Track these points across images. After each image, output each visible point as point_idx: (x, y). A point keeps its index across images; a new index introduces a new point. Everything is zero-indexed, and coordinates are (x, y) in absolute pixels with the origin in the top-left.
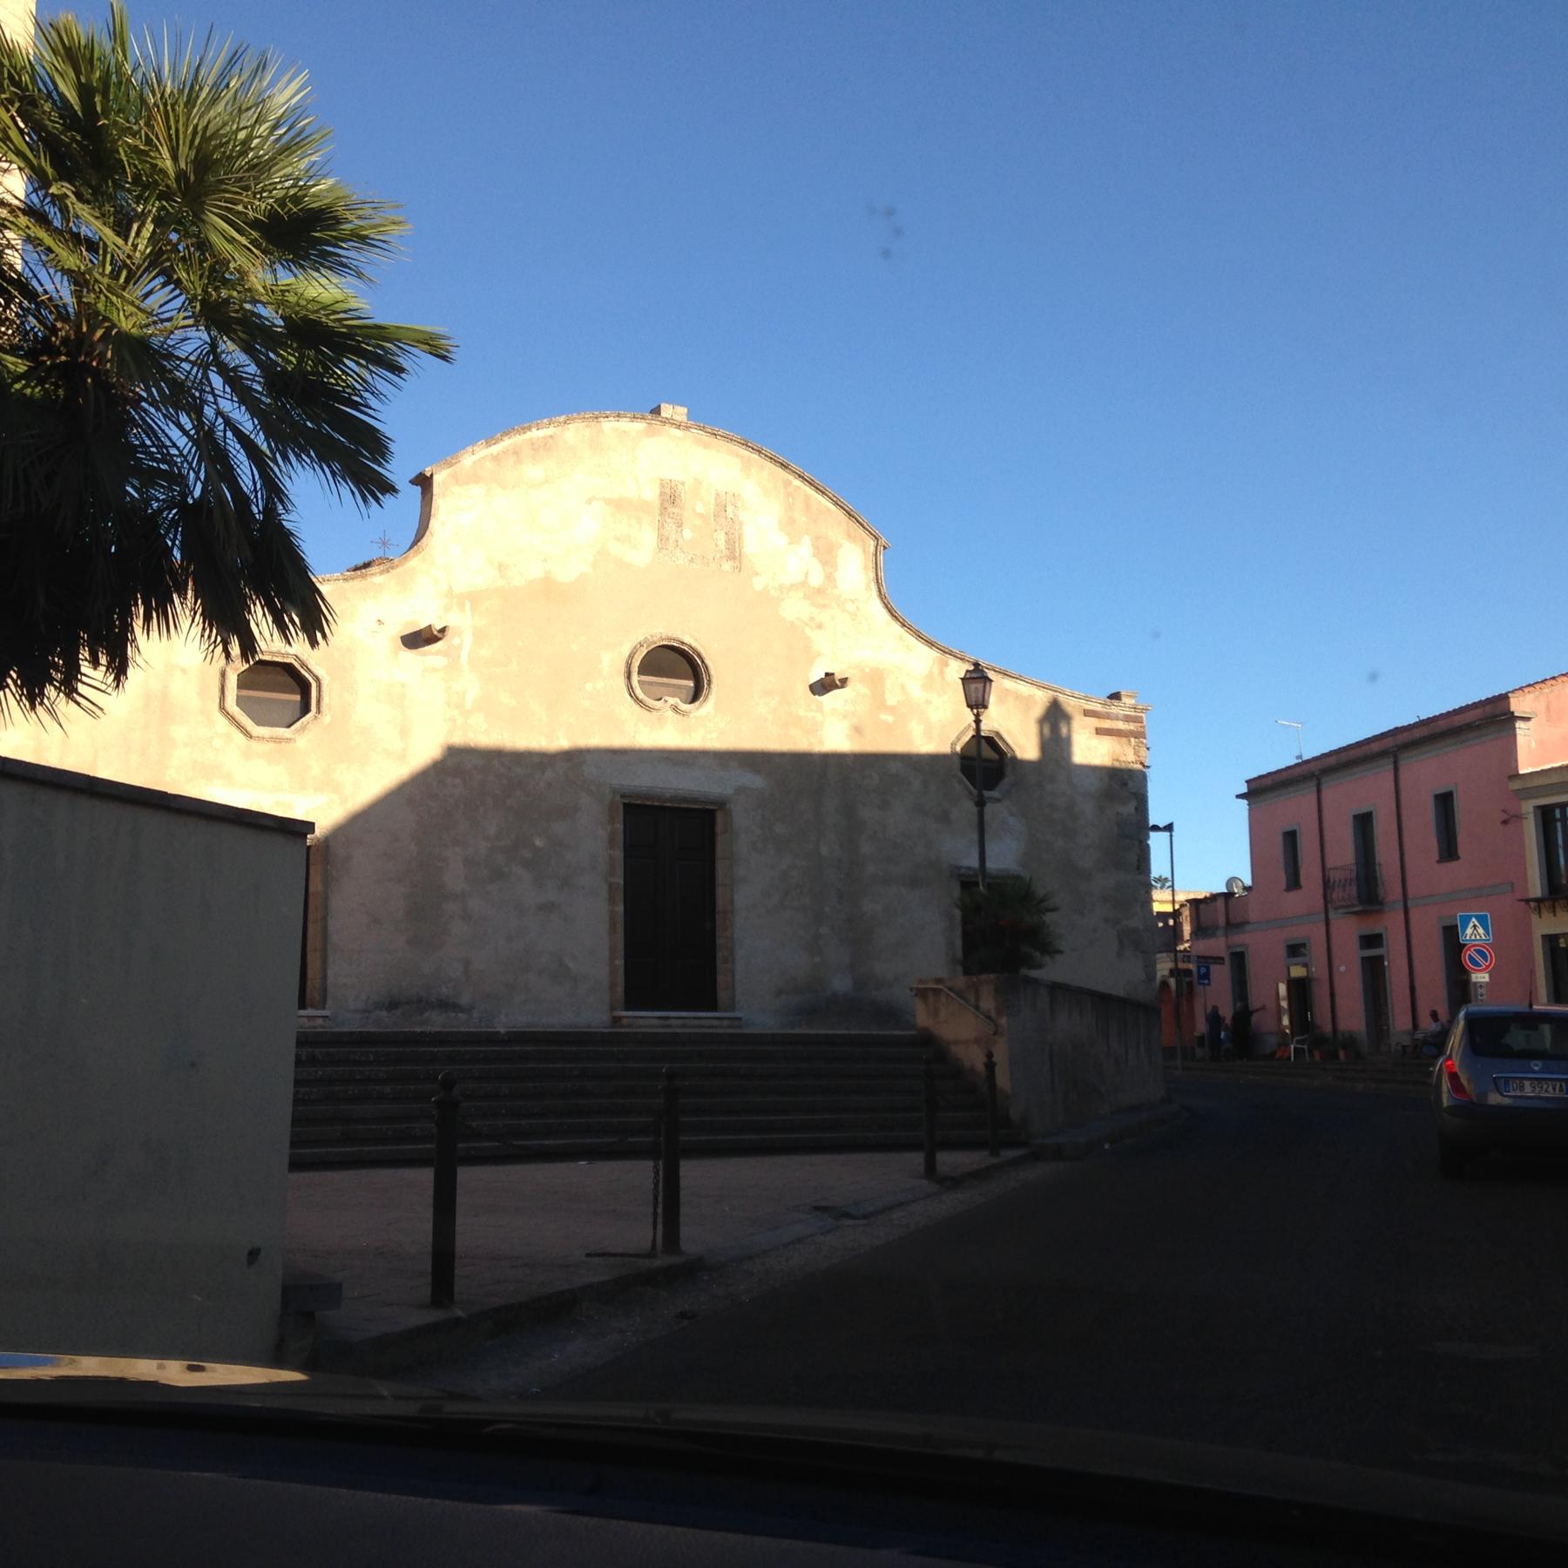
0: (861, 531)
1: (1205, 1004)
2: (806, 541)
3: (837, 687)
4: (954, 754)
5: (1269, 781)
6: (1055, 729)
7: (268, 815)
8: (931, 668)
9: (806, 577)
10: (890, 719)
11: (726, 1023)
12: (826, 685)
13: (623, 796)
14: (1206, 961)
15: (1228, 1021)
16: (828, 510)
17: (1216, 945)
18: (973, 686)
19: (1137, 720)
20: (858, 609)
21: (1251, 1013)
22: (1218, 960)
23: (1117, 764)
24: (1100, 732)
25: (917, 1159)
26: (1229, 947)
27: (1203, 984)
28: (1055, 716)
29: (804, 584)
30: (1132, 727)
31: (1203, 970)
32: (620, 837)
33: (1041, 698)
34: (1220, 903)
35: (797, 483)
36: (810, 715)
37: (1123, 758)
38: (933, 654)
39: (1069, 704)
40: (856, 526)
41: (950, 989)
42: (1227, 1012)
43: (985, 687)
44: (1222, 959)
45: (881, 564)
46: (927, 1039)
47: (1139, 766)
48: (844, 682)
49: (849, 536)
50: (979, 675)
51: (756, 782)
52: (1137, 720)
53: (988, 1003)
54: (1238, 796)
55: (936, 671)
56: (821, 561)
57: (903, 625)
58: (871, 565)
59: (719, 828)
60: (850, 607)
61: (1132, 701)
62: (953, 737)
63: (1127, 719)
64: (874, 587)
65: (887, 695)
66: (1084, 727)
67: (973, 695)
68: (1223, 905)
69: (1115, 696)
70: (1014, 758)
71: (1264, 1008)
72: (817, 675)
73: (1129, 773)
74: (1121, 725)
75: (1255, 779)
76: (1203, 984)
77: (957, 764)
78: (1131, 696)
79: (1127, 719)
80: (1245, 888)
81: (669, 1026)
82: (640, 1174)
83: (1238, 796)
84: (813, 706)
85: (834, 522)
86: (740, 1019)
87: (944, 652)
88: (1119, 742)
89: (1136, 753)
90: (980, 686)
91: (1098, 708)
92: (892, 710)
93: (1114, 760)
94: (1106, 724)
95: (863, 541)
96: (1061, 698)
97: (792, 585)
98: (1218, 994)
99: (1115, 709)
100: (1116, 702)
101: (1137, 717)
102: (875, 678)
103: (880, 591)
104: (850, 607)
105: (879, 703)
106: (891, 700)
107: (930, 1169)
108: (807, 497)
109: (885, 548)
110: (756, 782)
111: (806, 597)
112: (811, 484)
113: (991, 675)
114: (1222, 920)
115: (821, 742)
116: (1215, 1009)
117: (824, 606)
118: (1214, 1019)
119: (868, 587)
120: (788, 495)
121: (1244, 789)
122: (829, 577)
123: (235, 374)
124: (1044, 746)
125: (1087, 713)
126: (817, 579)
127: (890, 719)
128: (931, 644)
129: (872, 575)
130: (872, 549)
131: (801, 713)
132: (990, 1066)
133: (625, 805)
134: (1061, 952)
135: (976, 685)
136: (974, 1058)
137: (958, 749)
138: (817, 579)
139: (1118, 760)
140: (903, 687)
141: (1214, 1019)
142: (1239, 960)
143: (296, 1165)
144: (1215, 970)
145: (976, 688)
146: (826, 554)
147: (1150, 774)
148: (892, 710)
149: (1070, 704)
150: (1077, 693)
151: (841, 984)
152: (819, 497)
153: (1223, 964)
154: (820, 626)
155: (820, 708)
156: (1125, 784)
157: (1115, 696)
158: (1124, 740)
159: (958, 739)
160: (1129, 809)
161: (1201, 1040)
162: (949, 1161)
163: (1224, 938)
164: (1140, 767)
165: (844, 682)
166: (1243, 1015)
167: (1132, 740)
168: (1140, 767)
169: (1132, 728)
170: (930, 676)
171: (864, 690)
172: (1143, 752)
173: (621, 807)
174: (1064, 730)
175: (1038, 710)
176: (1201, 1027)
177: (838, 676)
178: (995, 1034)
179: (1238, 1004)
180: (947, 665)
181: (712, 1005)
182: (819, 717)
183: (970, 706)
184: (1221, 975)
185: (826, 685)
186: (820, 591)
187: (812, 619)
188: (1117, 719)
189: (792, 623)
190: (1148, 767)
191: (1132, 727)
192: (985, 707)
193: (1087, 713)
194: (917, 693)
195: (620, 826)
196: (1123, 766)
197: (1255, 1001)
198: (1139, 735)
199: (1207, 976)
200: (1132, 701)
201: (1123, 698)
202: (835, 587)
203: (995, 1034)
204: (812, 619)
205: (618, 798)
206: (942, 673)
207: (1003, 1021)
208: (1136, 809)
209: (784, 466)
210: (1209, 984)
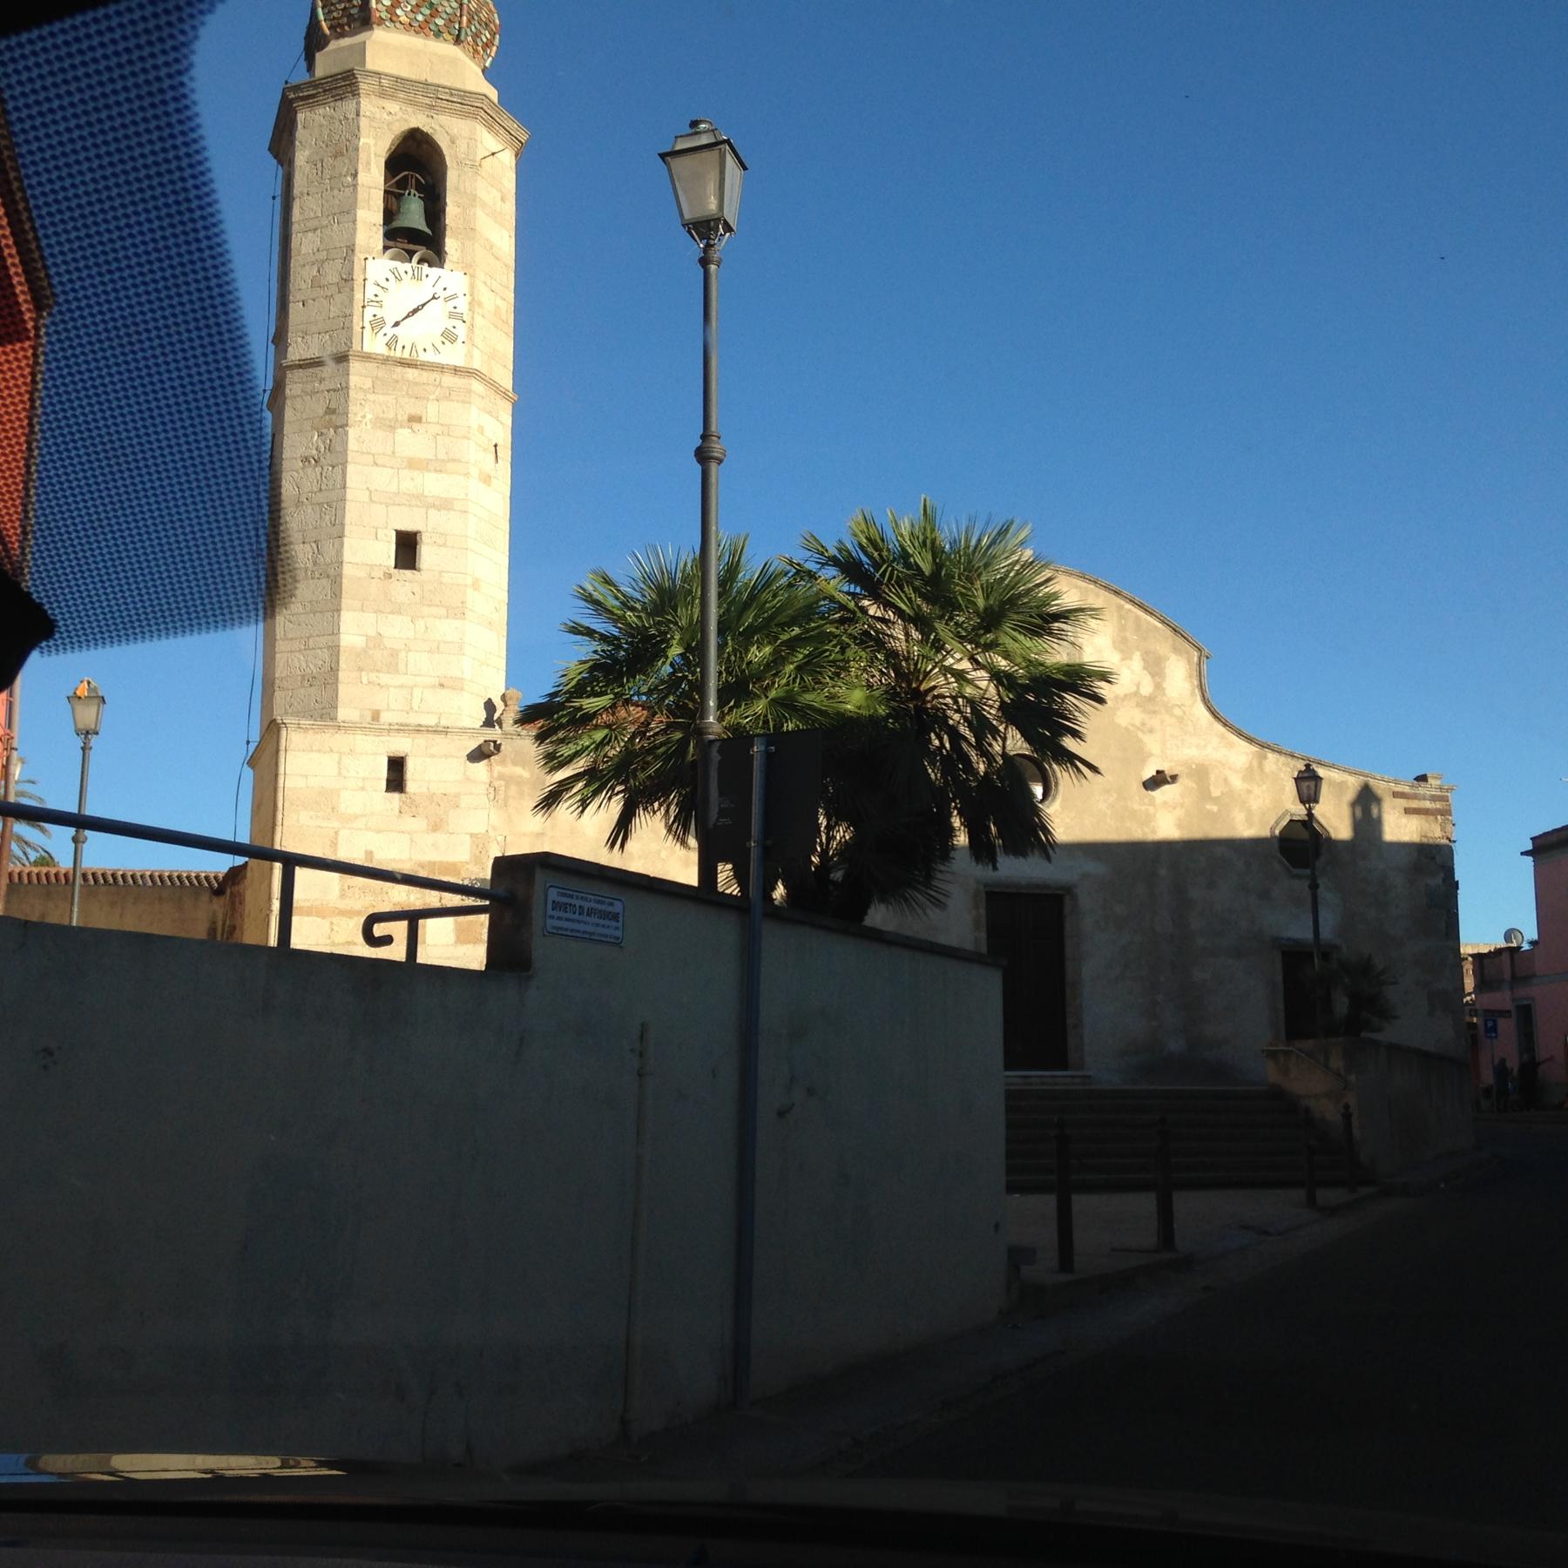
0: (1187, 646)
1: (1493, 1056)
2: (1137, 656)
3: (1168, 783)
4: (1273, 837)
5: (1554, 839)
6: (1367, 812)
7: (150, 839)
8: (1251, 762)
9: (1138, 688)
10: (1215, 808)
11: (1077, 1080)
12: (1158, 781)
13: (986, 885)
14: (1492, 1015)
15: (1515, 1072)
16: (1156, 627)
17: (1501, 999)
18: (1305, 784)
19: (1444, 799)
20: (1184, 713)
21: (1539, 1064)
22: (1504, 1013)
23: (1425, 840)
24: (1408, 811)
25: (1300, 1194)
26: (1513, 1000)
27: (1491, 1037)
28: (1366, 800)
29: (1136, 693)
30: (1438, 805)
31: (1490, 1024)
32: (983, 920)
33: (1353, 783)
34: (1505, 957)
35: (1128, 606)
36: (1143, 808)
37: (1430, 835)
38: (1254, 749)
39: (1379, 787)
40: (1180, 640)
41: (1300, 1050)
42: (1513, 1064)
43: (1316, 786)
44: (1509, 1012)
45: (1205, 672)
46: (1277, 1094)
47: (1445, 841)
48: (1174, 778)
49: (1176, 650)
50: (1311, 774)
51: (1092, 867)
52: (1444, 799)
53: (1337, 1062)
54: (1522, 854)
55: (1255, 764)
56: (1150, 673)
57: (1225, 725)
58: (1195, 674)
59: (1067, 910)
60: (1177, 712)
61: (1438, 782)
62: (1272, 822)
63: (1434, 799)
64: (1197, 692)
65: (1212, 788)
66: (1394, 808)
67: (1305, 791)
68: (1508, 961)
69: (1422, 778)
70: (1329, 839)
71: (1551, 1059)
72: (1149, 773)
73: (1438, 847)
74: (1428, 804)
75: (1540, 836)
76: (1491, 1037)
77: (1276, 845)
78: (1436, 778)
79: (1434, 799)
80: (1532, 943)
81: (1030, 1084)
82: (1146, 1203)
83: (1522, 854)
84: (1146, 801)
85: (1163, 641)
86: (1089, 1076)
87: (1262, 746)
88: (1427, 821)
89: (1443, 829)
90: (1312, 784)
91: (1407, 789)
92: (1216, 800)
93: (1422, 836)
94: (1414, 804)
95: (1188, 653)
96: (1372, 782)
97: (1126, 695)
98: (1505, 1047)
99: (1422, 790)
100: (1422, 784)
101: (1442, 797)
102: (1201, 773)
103: (1203, 696)
104: (1177, 712)
105: (1204, 794)
106: (1216, 792)
107: (1311, 1201)
108: (1137, 618)
109: (1207, 658)
110: (1092, 867)
111: (1138, 705)
112: (1141, 606)
113: (1321, 772)
114: (1507, 975)
115: (1154, 831)
116: (1503, 1061)
117: (1154, 712)
118: (1501, 1071)
119: (1193, 693)
120: (1121, 617)
121: (1530, 847)
122: (1158, 687)
123: (1049, 703)
124: (1357, 826)
125: (1396, 795)
126: (1147, 688)
127: (1215, 808)
128: (1250, 740)
129: (1196, 683)
130: (1196, 659)
131: (1136, 806)
132: (1347, 1116)
133: (987, 893)
134: (1396, 1017)
135: (1308, 784)
136: (1329, 1112)
137: (1277, 832)
138: (1147, 688)
139: (1426, 837)
140: (1226, 780)
141: (1501, 1071)
142: (1525, 1013)
143: (1011, 1188)
144: (1503, 1024)
145: (1308, 787)
146: (1155, 667)
147: (1457, 848)
148: (1216, 800)
149: (1380, 787)
150: (1386, 778)
151: (1175, 1045)
152: (1149, 618)
153: (1511, 1016)
154: (1151, 731)
155: (1152, 802)
156: (1433, 858)
157: (1422, 778)
158: (1432, 818)
159: (1277, 823)
160: (1437, 881)
161: (1488, 1091)
162: (1327, 1196)
163: (1509, 993)
164: (1447, 842)
165: (1174, 778)
166: (1530, 1067)
167: (1439, 817)
168: (1447, 842)
169: (1438, 806)
170: (1250, 769)
171: (1192, 784)
172: (1449, 827)
173: (984, 896)
174: (1375, 812)
175: (1350, 795)
176: (1488, 1077)
177: (1168, 773)
178: (1344, 1089)
179: (1525, 1056)
180: (1265, 757)
181: (1063, 1064)
182: (1151, 810)
183: (1303, 802)
184: (1507, 1026)
185: (1158, 781)
186: (1151, 699)
187: (1143, 724)
188: (1424, 799)
189: (1126, 728)
190: (1454, 842)
191: (1438, 805)
192: (1317, 801)
193: (1396, 795)
194: (1237, 783)
195: (983, 911)
196: (1431, 841)
197: (1542, 1054)
198: (1446, 812)
199: (1494, 1029)
200: (1438, 782)
201: (1429, 780)
202: (1164, 694)
203: (1344, 1089)
204: (1143, 724)
205: (981, 887)
206: (1261, 766)
207: (1352, 1078)
208: (1444, 880)
209: (1117, 593)
210: (1496, 1037)
